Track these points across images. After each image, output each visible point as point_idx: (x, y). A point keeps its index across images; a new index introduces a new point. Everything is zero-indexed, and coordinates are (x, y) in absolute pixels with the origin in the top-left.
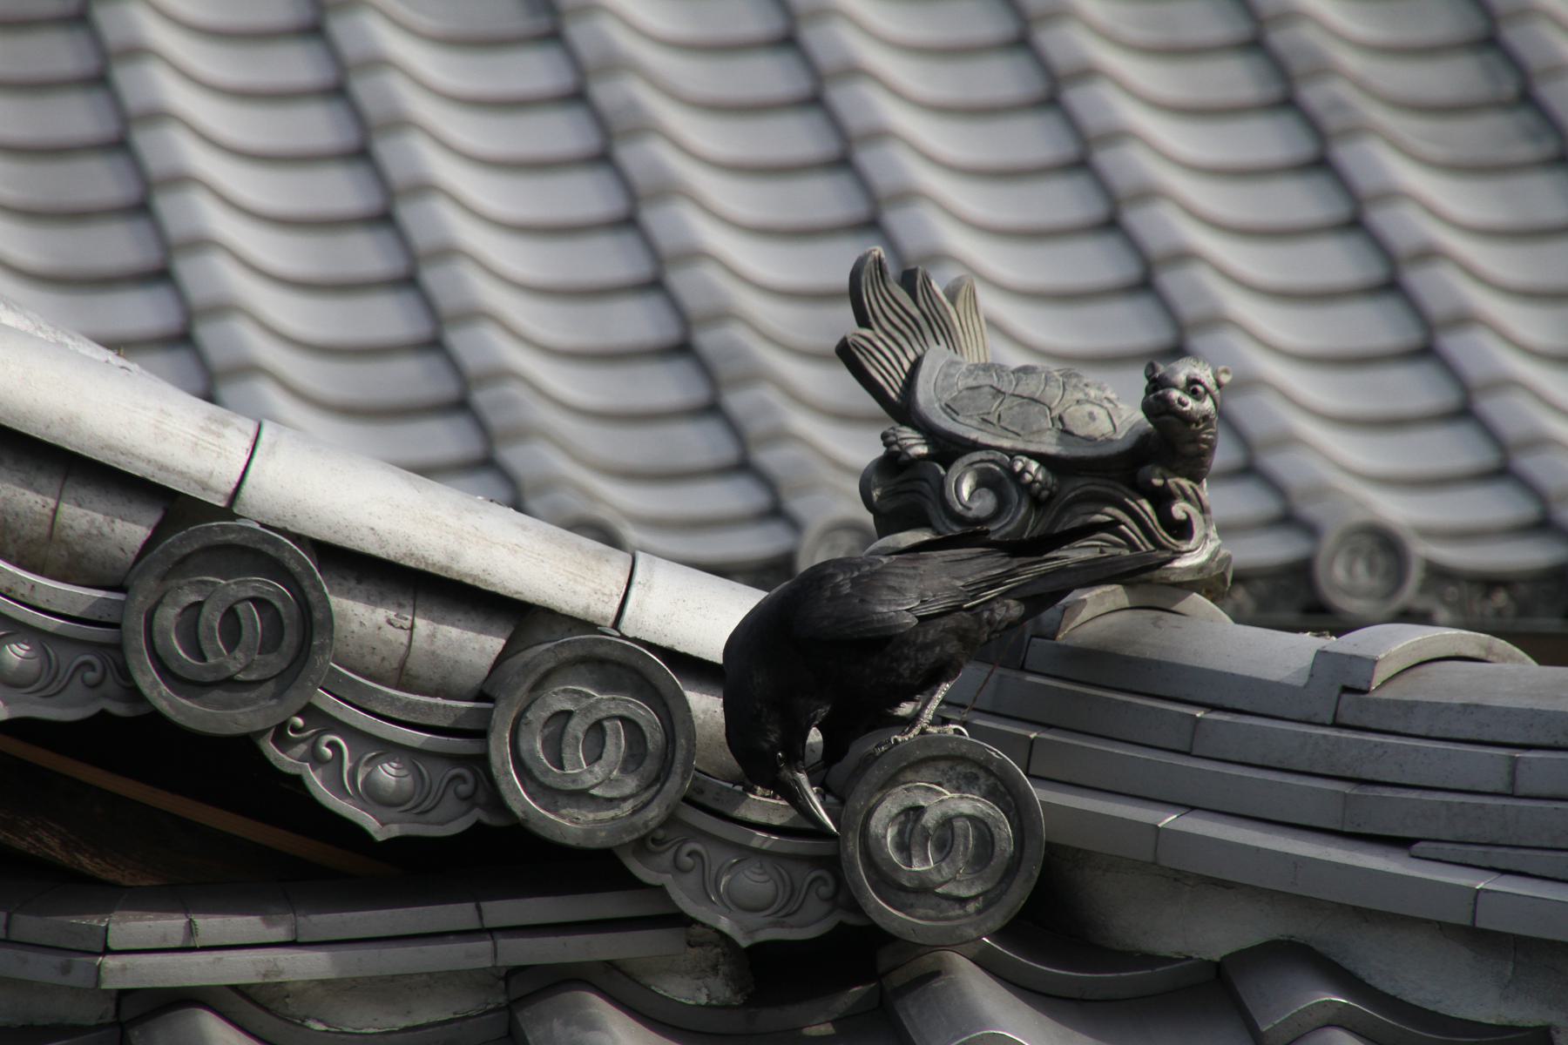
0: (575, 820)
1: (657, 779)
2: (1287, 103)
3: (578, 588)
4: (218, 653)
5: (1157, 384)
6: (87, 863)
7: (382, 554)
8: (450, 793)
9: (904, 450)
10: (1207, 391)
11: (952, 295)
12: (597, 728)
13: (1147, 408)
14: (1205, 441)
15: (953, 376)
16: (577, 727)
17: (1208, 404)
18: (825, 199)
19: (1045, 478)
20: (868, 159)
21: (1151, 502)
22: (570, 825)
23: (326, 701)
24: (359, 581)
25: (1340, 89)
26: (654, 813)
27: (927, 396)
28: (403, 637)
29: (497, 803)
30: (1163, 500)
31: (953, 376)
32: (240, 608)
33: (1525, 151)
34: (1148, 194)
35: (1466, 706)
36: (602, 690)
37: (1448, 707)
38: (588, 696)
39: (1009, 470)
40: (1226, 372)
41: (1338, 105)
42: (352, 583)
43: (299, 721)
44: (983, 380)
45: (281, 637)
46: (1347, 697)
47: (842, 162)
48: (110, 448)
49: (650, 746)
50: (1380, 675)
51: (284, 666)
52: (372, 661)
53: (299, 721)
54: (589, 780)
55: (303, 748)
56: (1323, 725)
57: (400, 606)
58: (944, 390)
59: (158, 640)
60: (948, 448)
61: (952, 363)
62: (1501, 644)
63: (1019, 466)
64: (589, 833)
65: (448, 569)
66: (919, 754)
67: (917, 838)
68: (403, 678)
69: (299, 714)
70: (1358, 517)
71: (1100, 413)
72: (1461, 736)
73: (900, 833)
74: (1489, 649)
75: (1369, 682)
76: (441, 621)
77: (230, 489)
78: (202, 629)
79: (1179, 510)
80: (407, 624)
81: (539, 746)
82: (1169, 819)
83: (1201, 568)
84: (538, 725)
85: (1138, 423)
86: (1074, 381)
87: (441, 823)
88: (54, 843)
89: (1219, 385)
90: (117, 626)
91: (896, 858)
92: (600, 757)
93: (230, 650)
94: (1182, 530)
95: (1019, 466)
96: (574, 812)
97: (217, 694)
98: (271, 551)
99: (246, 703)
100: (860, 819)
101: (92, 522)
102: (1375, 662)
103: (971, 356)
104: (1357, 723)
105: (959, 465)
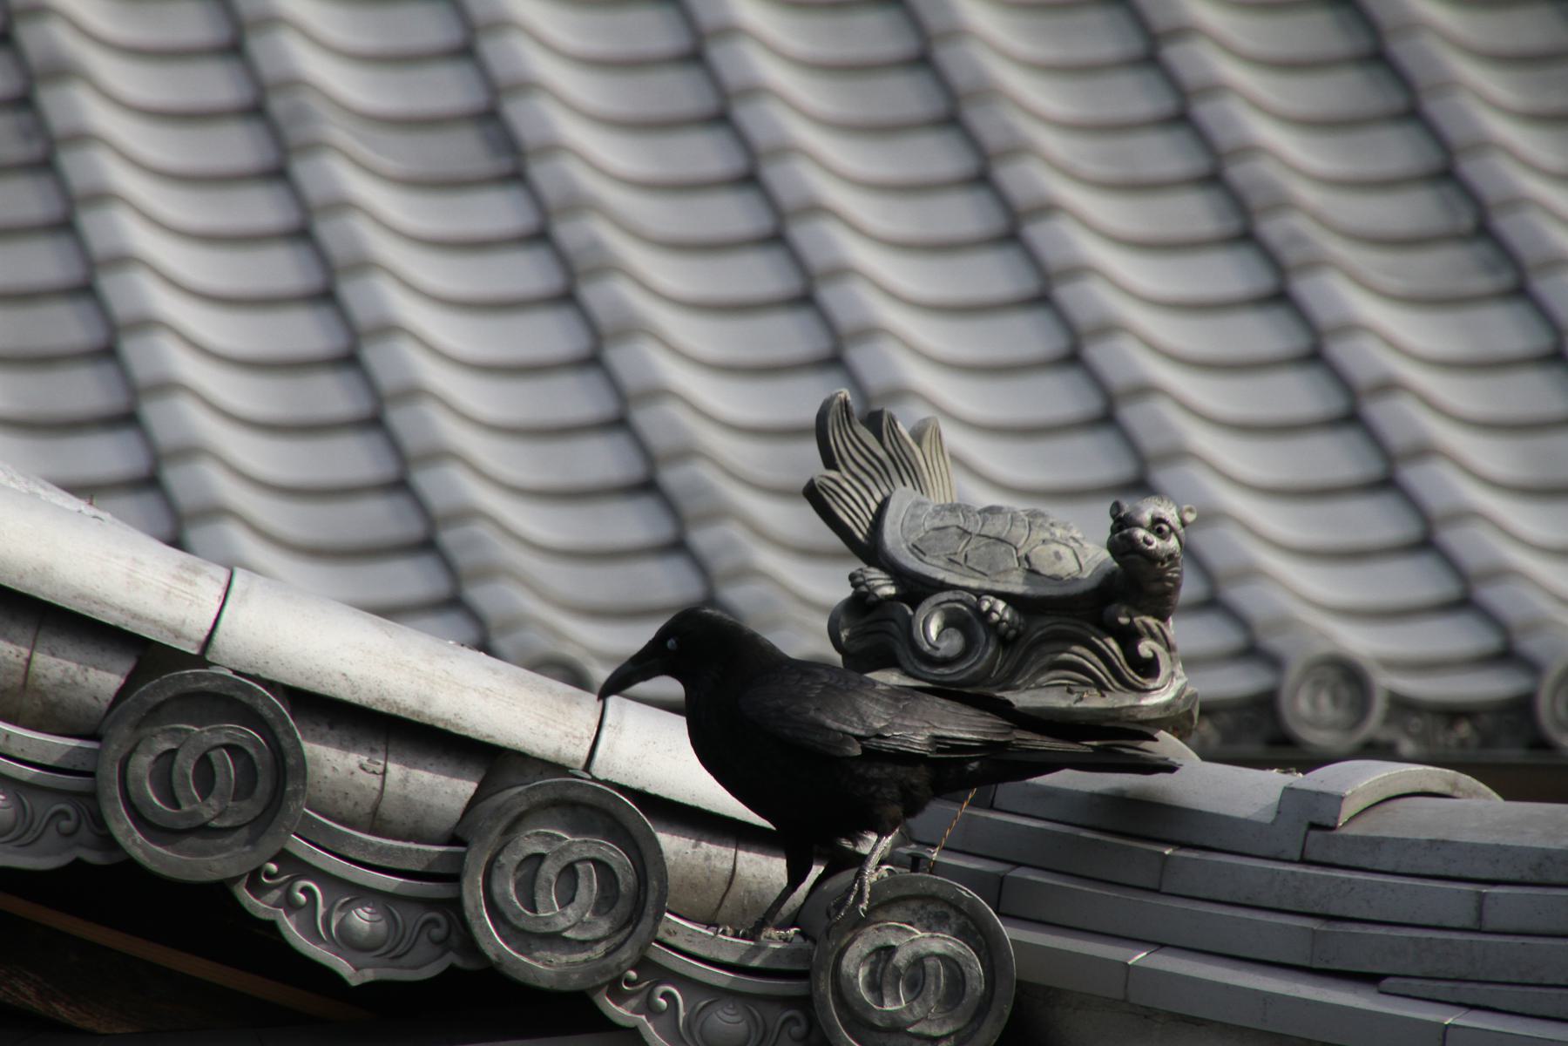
0: (548, 963)
1: (629, 922)
2: (1246, 237)
3: (550, 731)
4: (192, 801)
5: (1122, 523)
6: (62, 1011)
7: (354, 699)
8: (424, 937)
9: (871, 591)
10: (1172, 530)
11: (918, 436)
12: (569, 871)
13: (1112, 547)
14: (1171, 580)
15: (919, 517)
16: (550, 870)
17: (1173, 543)
18: (789, 336)
19: (1012, 617)
20: (830, 295)
21: (1117, 640)
22: (544, 968)
23: (300, 847)
24: (331, 727)
25: (1299, 223)
26: (627, 954)
27: (894, 537)
28: (375, 782)
29: (470, 945)
30: (1128, 638)
31: (919, 517)
32: (213, 755)
33: (1483, 283)
34: (1109, 329)
35: (1431, 842)
36: (574, 831)
37: (1416, 843)
38: (560, 839)
39: (976, 609)
40: (1190, 510)
41: (1297, 239)
42: (324, 729)
43: (273, 867)
44: (950, 520)
45: (254, 784)
46: (1314, 834)
47: (805, 300)
48: (83, 597)
49: (622, 888)
50: (1347, 811)
51: (258, 812)
52: (346, 806)
53: (273, 867)
54: (562, 923)
55: (276, 895)
56: (1291, 861)
57: (373, 750)
58: (911, 530)
59: (132, 788)
60: (916, 589)
61: (918, 504)
62: (1466, 780)
63: (986, 606)
64: (563, 976)
65: (419, 713)
66: (890, 894)
67: (889, 978)
68: (376, 822)
69: (272, 861)
70: (1322, 648)
71: (1066, 553)
72: (1428, 872)
73: (872, 973)
74: (1455, 785)
75: (1336, 818)
76: (414, 766)
77: (202, 637)
78: (176, 777)
79: (1146, 648)
80: (380, 769)
81: (511, 889)
82: (1139, 957)
83: (1167, 706)
84: (510, 868)
85: (1104, 562)
86: (1040, 521)
87: (415, 968)
88: (30, 992)
89: (1184, 524)
90: (91, 774)
91: (867, 998)
92: (572, 900)
93: (203, 797)
94: (1149, 668)
95: (986, 606)
96: (547, 955)
97: (192, 841)
98: (245, 699)
99: (220, 850)
100: (832, 959)
101: (66, 671)
102: (1342, 798)
103: (938, 496)
104: (1324, 860)
105: (926, 606)
